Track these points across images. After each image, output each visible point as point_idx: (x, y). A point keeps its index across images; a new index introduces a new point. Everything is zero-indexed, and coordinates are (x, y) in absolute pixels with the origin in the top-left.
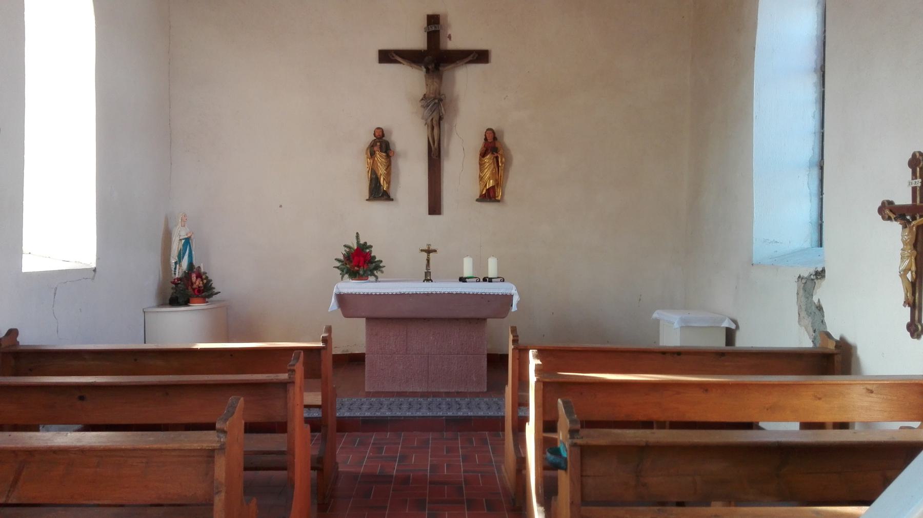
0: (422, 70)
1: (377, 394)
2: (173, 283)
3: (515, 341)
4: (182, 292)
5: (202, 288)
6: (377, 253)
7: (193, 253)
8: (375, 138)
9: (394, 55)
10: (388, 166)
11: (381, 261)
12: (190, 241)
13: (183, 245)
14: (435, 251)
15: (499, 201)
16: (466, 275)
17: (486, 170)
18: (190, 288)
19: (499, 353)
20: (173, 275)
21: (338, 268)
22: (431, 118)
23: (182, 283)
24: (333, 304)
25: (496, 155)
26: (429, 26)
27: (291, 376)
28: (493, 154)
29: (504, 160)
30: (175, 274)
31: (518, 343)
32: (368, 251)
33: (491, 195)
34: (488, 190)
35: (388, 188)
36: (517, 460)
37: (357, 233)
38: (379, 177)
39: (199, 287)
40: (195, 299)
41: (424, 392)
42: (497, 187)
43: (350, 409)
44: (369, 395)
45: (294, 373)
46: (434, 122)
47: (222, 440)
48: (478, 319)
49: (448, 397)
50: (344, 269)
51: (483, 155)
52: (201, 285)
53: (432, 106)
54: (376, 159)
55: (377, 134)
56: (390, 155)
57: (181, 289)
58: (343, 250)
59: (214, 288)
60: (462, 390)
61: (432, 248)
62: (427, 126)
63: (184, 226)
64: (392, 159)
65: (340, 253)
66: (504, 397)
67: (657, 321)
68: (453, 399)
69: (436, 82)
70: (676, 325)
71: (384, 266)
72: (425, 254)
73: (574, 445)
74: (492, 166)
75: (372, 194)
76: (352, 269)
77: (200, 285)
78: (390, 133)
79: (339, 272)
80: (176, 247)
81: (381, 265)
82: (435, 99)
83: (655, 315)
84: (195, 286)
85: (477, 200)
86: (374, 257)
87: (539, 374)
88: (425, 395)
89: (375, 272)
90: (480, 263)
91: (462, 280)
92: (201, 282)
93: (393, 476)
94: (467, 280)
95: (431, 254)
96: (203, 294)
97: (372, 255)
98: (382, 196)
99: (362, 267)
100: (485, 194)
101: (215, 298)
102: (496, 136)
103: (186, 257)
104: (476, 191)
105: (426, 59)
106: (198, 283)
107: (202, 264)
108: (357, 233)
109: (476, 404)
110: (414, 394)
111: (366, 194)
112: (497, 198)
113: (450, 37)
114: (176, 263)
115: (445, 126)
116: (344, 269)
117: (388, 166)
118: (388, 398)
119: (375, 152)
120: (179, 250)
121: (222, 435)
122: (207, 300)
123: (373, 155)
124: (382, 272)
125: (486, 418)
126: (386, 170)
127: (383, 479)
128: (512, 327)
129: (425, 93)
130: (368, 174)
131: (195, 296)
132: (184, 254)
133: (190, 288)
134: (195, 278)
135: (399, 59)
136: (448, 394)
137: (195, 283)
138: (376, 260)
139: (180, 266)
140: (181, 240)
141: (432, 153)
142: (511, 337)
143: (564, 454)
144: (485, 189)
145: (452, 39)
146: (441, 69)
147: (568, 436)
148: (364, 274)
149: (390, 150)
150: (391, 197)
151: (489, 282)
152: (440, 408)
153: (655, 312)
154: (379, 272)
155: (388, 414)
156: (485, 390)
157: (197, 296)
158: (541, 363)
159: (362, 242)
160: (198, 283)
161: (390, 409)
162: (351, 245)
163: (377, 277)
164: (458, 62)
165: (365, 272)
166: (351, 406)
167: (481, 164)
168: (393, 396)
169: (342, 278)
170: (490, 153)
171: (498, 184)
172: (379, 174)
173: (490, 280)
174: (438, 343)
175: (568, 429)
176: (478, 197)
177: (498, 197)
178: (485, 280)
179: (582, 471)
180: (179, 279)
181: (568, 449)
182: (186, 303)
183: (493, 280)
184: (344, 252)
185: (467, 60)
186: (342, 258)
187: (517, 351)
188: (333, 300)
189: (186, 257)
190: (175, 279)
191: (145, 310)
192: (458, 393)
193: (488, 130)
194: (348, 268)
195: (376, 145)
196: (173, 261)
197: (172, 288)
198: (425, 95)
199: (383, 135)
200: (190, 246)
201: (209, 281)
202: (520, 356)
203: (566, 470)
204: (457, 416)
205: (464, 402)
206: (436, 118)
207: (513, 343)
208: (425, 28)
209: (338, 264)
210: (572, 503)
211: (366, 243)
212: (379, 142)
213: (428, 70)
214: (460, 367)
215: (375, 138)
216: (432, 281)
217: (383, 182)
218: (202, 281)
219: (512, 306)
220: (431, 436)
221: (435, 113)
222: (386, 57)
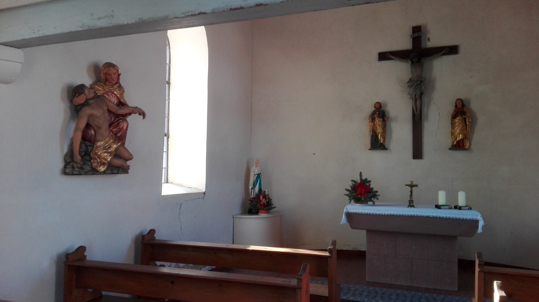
0: (408, 63)
2: (250, 200)
5: (266, 204)
8: (375, 109)
9: (389, 55)
10: (384, 127)
12: (260, 176)
14: (416, 186)
15: (467, 149)
17: (456, 128)
18: (259, 204)
21: (347, 195)
22: (414, 94)
24: (344, 219)
25: (464, 117)
26: (414, 34)
28: (462, 116)
29: (470, 120)
32: (368, 184)
33: (461, 145)
34: (458, 142)
35: (384, 141)
37: (361, 172)
38: (377, 134)
39: (264, 204)
42: (466, 139)
46: (417, 97)
50: (351, 196)
51: (454, 117)
52: (265, 202)
54: (375, 122)
55: (376, 107)
58: (351, 183)
59: (273, 204)
61: (414, 183)
64: (387, 122)
65: (349, 185)
72: (409, 188)
74: (461, 125)
78: (386, 105)
79: (348, 198)
80: (252, 179)
81: (377, 194)
82: (417, 81)
84: (262, 203)
85: (450, 149)
86: (372, 189)
89: (373, 199)
90: (452, 195)
91: (438, 207)
97: (371, 187)
98: (380, 147)
103: (258, 185)
104: (449, 143)
106: (264, 201)
107: (267, 190)
108: (361, 172)
110: (401, 287)
111: (369, 146)
112: (465, 148)
113: (429, 39)
114: (252, 189)
115: (425, 99)
123: (374, 120)
124: (378, 199)
126: (382, 130)
133: (259, 204)
134: (262, 198)
135: (392, 57)
139: (254, 190)
140: (255, 175)
144: (456, 141)
145: (430, 40)
146: (422, 60)
154: (375, 199)
156: (457, 289)
157: (263, 209)
159: (364, 178)
160: (264, 201)
163: (374, 202)
165: (365, 199)
170: (460, 116)
172: (378, 133)
173: (460, 208)
176: (450, 147)
177: (466, 146)
180: (253, 198)
182: (257, 213)
185: (440, 54)
186: (350, 188)
189: (258, 185)
194: (353, 195)
195: (376, 113)
199: (381, 107)
201: (270, 200)
206: (419, 93)
209: (347, 193)
211: (366, 179)
213: (412, 63)
215: (375, 109)
216: (414, 207)
217: (381, 138)
218: (266, 200)
221: (418, 90)
222: (383, 56)
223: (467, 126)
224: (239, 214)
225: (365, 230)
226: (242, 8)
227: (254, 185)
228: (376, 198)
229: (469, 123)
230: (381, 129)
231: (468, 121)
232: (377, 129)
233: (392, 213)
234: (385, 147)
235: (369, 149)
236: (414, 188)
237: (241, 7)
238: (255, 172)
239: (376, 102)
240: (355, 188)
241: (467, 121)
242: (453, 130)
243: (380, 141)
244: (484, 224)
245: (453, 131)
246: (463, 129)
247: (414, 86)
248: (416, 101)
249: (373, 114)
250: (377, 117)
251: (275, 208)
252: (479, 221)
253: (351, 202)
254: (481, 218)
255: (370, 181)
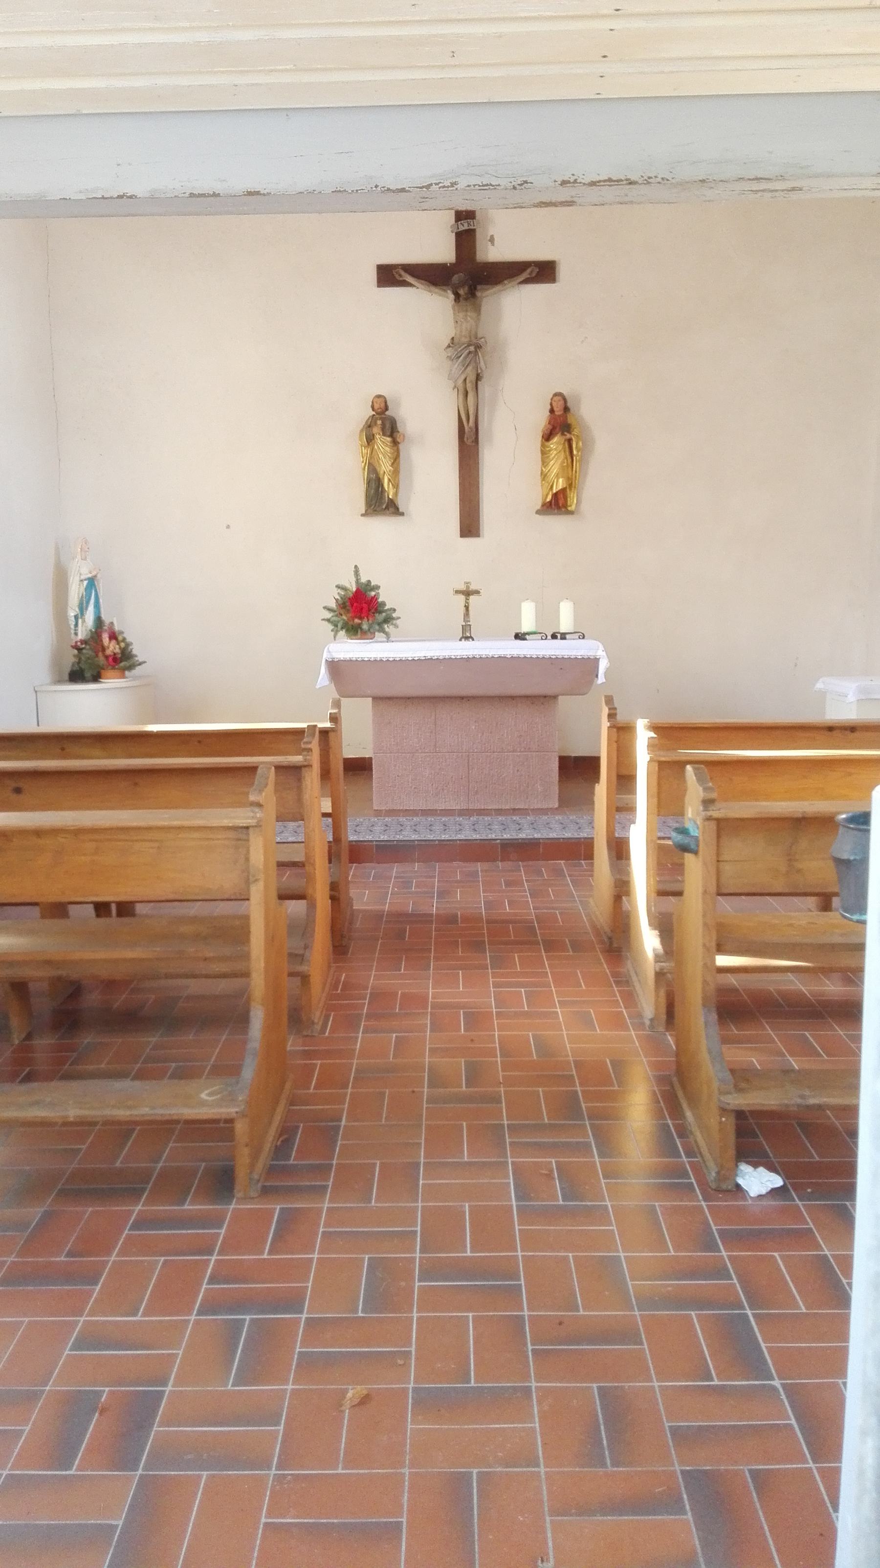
0: (447, 298)
1: (391, 813)
2: (75, 647)
3: (612, 716)
4: (89, 661)
5: (119, 656)
6: (384, 596)
7: (101, 601)
8: (374, 413)
9: (402, 273)
10: (396, 460)
11: (394, 610)
12: (96, 583)
13: (86, 589)
14: (477, 592)
15: (571, 513)
16: (525, 629)
17: (552, 463)
18: (100, 654)
19: (573, 755)
20: (73, 636)
21: (328, 620)
22: (463, 377)
23: (88, 647)
24: (323, 677)
25: (568, 436)
27: (308, 757)
28: (563, 434)
29: (580, 444)
30: (76, 634)
31: (616, 719)
33: (561, 503)
34: (555, 495)
35: (396, 494)
36: (615, 883)
37: (356, 567)
38: (381, 477)
39: (115, 654)
40: (111, 673)
41: (463, 810)
42: (570, 490)
43: (356, 831)
44: (378, 813)
45: (310, 753)
46: (469, 386)
47: (258, 815)
48: (545, 697)
49: (500, 815)
50: (338, 622)
51: (548, 437)
52: (117, 650)
53: (465, 358)
54: (376, 447)
55: (376, 406)
56: (399, 440)
57: (87, 656)
58: (336, 594)
59: (136, 656)
60: (521, 806)
61: (473, 587)
62: (456, 390)
63: (85, 559)
64: (401, 446)
65: (331, 598)
66: (593, 810)
67: (823, 694)
68: (509, 818)
69: (470, 317)
70: (851, 698)
71: (399, 618)
73: (709, 819)
74: (562, 455)
75: (370, 506)
76: (351, 623)
77: (115, 651)
79: (330, 627)
80: (75, 591)
81: (394, 615)
82: (469, 345)
83: (819, 685)
84: (109, 652)
85: (538, 512)
86: (383, 604)
87: (653, 751)
88: (463, 813)
90: (546, 611)
91: (519, 636)
92: (117, 646)
93: (433, 914)
94: (527, 637)
95: (471, 597)
96: (122, 664)
97: (380, 600)
98: (387, 508)
99: (366, 619)
100: (550, 502)
101: (137, 671)
102: (569, 404)
103: (91, 608)
104: (537, 496)
105: (456, 279)
106: (112, 648)
107: (115, 618)
108: (356, 567)
109: (545, 823)
111: (362, 506)
112: (569, 508)
113: (492, 240)
114: (76, 617)
115: (485, 388)
116: (338, 622)
117: (396, 460)
118: (411, 818)
119: (373, 435)
120: (80, 595)
121: (257, 810)
122: (127, 673)
123: (371, 440)
124: (396, 626)
125: (562, 840)
127: (421, 919)
128: (606, 697)
129: (453, 335)
130: (364, 473)
131: (110, 667)
132: (88, 602)
133: (100, 654)
134: (107, 639)
135: (410, 279)
136: (499, 812)
137: (108, 648)
138: (386, 608)
139: (84, 621)
140: (82, 581)
141: (466, 436)
142: (605, 711)
143: (694, 832)
144: (551, 493)
145: (496, 242)
146: (478, 294)
147: (701, 808)
148: (369, 630)
149: (398, 432)
150: (401, 510)
151: (562, 639)
152: (490, 829)
153: (821, 680)
154: (391, 627)
155: (414, 837)
156: (556, 805)
157: (113, 668)
158: (655, 736)
159: (364, 580)
160: (112, 648)
161: (415, 830)
162: (348, 585)
163: (387, 635)
164: (506, 282)
165: (370, 627)
166: (358, 828)
167: (543, 453)
168: (417, 815)
169: (335, 637)
170: (559, 435)
171: (570, 485)
172: (382, 472)
173: (563, 636)
174: (483, 734)
175: (701, 799)
176: (539, 507)
177: (571, 506)
178: (554, 637)
179: (718, 854)
180: (83, 642)
181: (701, 827)
182: (96, 678)
183: (567, 636)
184: (338, 597)
186: (333, 605)
187: (615, 730)
188: (323, 669)
189: (91, 608)
190: (76, 642)
191: (36, 689)
192: (514, 810)
193: (556, 395)
194: (344, 620)
195: (376, 424)
196: (72, 614)
197: (74, 656)
198: (453, 339)
199: (386, 408)
200: (96, 591)
201: (128, 645)
202: (618, 737)
203: (696, 853)
204: (518, 839)
205: (526, 821)
206: (472, 377)
207: (608, 718)
208: (451, 227)
209: (329, 615)
210: (705, 892)
211: (369, 581)
212: (380, 419)
213: (457, 297)
214: (518, 771)
215: (374, 413)
216: (473, 640)
217: (389, 485)
218: (118, 643)
219: (597, 676)
220: (479, 866)
221: (470, 368)
223: (574, 458)
224: (47, 684)
225: (369, 697)
226: (215, 195)
227: (82, 608)
228: (392, 624)
229: (578, 452)
230: (390, 463)
231: (577, 447)
232: (378, 462)
233: (429, 654)
234: (397, 509)
235: (363, 515)
236: (472, 598)
237: (214, 193)
238: (80, 574)
239: (374, 395)
240: (344, 603)
241: (574, 446)
242: (545, 467)
243: (386, 494)
244: (608, 665)
245: (544, 469)
246: (565, 464)
247: (461, 358)
248: (466, 394)
249: (369, 426)
250: (379, 434)
251: (144, 665)
252: (599, 659)
253: (337, 637)
254: (604, 653)
255: (378, 587)
